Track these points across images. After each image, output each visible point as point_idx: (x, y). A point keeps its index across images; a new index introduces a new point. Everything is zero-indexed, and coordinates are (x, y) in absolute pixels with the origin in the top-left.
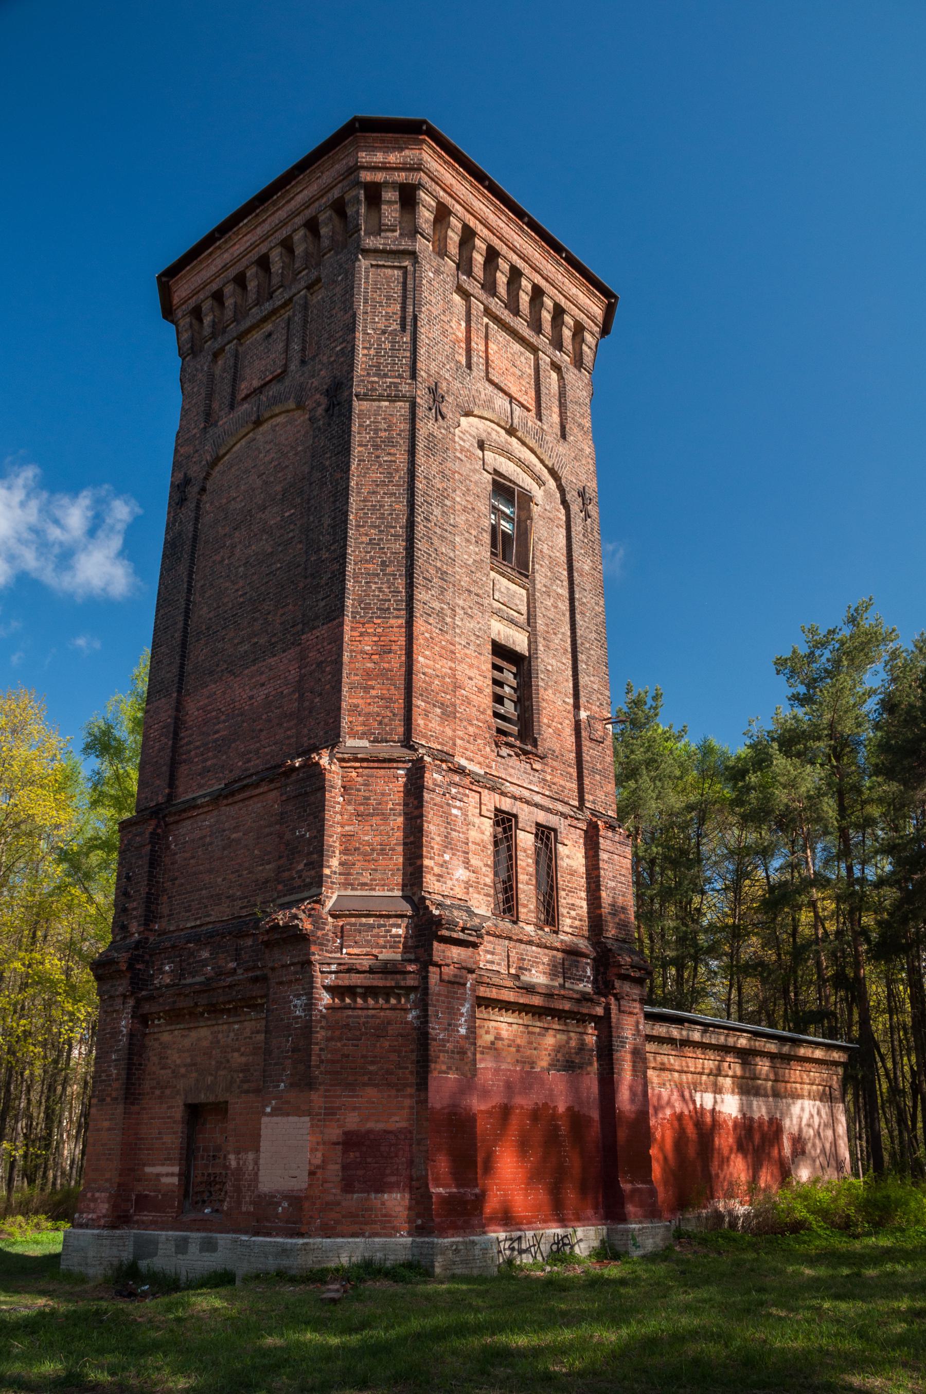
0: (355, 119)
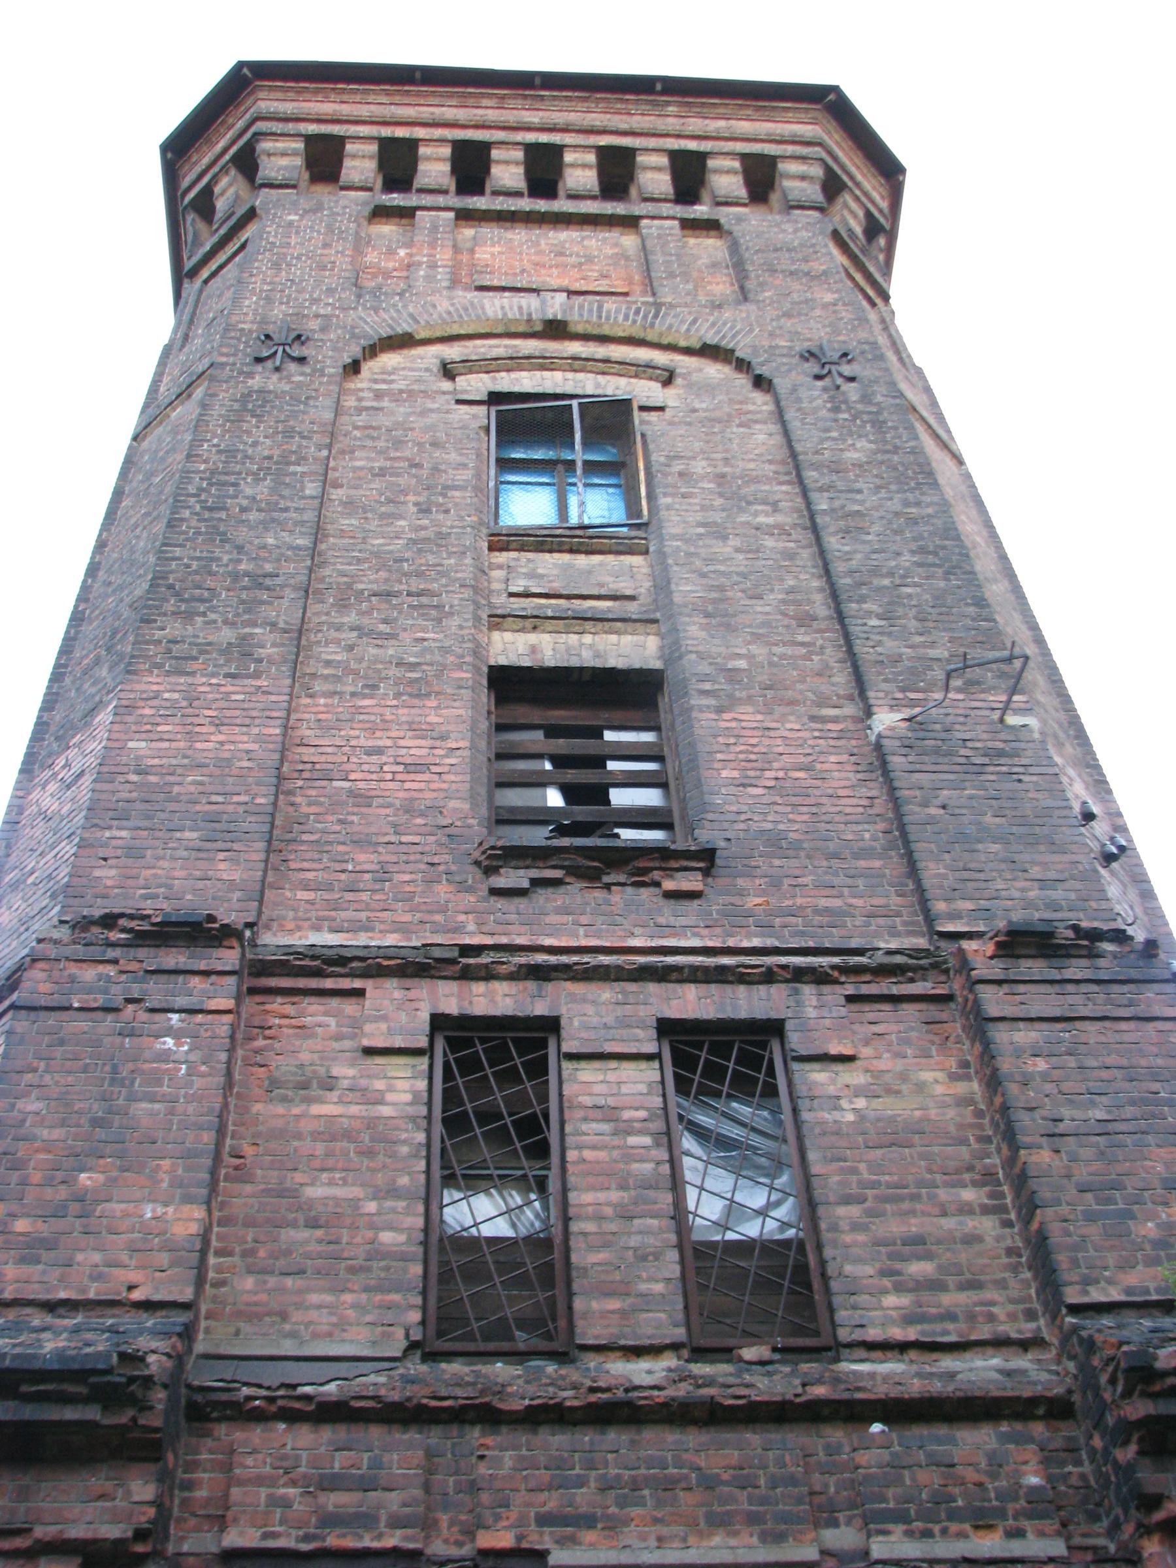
0: (241, 65)
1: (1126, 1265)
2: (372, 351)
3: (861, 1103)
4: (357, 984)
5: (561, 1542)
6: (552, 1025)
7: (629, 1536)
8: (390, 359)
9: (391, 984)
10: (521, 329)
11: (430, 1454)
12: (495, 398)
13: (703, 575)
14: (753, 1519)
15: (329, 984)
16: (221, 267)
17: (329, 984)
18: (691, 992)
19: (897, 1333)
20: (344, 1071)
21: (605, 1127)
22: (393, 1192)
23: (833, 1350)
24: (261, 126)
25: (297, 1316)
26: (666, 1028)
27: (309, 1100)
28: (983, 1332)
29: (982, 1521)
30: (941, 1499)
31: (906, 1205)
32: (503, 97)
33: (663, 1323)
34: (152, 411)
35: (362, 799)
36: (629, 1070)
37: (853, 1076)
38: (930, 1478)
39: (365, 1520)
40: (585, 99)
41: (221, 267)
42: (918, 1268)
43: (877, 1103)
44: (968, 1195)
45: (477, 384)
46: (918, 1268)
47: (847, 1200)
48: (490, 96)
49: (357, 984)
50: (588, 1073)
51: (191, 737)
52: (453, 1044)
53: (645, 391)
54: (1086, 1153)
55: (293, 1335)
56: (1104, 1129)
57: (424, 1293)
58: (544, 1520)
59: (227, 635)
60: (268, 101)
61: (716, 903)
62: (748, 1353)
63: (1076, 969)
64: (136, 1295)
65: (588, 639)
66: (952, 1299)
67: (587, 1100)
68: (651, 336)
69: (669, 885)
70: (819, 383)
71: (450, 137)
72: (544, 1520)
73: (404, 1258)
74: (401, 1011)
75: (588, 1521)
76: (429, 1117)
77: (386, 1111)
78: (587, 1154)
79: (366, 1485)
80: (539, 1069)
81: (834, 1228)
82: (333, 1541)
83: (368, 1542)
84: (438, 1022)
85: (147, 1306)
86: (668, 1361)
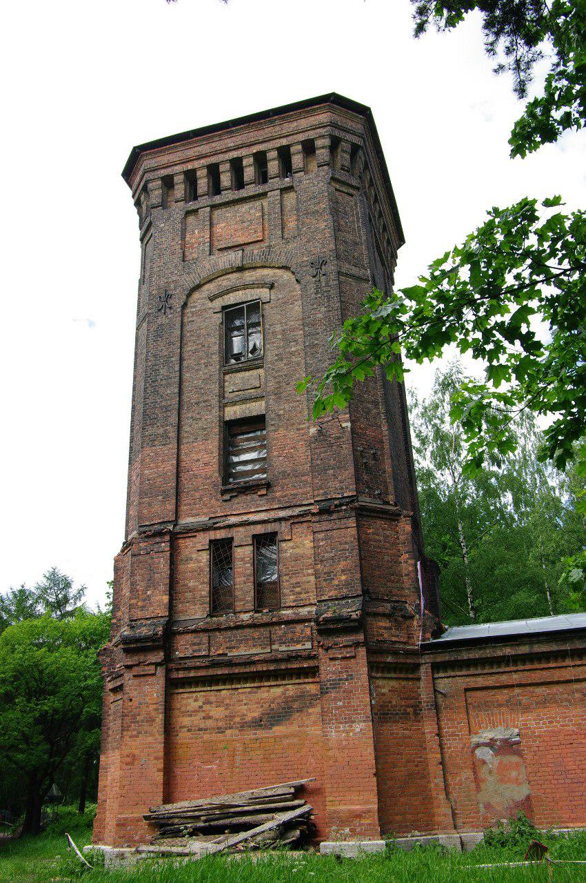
0: (135, 148)
1: (330, 591)
2: (189, 296)
3: (291, 551)
4: (195, 534)
5: (230, 652)
6: (232, 538)
7: (240, 650)
8: (196, 295)
9: (201, 533)
10: (230, 271)
11: (209, 637)
12: (224, 308)
13: (275, 378)
14: (261, 645)
15: (190, 535)
16: (148, 241)
17: (190, 535)
18: (259, 526)
19: (292, 604)
20: (194, 556)
21: (242, 563)
22: (203, 583)
23: (280, 608)
24: (147, 176)
25: (189, 611)
26: (254, 536)
27: (188, 564)
28: (308, 602)
29: (298, 642)
30: (292, 639)
31: (297, 575)
32: (220, 135)
33: (250, 606)
34: (145, 227)
35: (196, 476)
36: (247, 548)
37: (290, 544)
38: (290, 636)
39: (200, 650)
40: (248, 127)
41: (148, 241)
42: (298, 589)
43: (294, 551)
44: (310, 571)
45: (218, 303)
46: (298, 589)
47: (286, 575)
48: (216, 136)
49: (195, 534)
50: (239, 550)
51: (157, 467)
52: (215, 545)
53: (264, 293)
54: (327, 565)
55: (189, 615)
56: (332, 558)
57: (210, 604)
58: (227, 648)
59: (161, 431)
60: (147, 163)
61: (270, 495)
62: (265, 611)
63: (335, 516)
64: (159, 615)
65: (248, 405)
66: (303, 596)
67: (239, 557)
68: (267, 265)
69: (259, 493)
70: (314, 279)
71: (205, 164)
72: (227, 648)
73: (206, 597)
74: (203, 539)
75: (234, 648)
76: (210, 565)
77: (202, 564)
78: (238, 570)
79: (199, 644)
80: (231, 548)
81: (283, 581)
82: (195, 654)
83: (200, 654)
84: (211, 541)
85: (161, 617)
86: (251, 614)
